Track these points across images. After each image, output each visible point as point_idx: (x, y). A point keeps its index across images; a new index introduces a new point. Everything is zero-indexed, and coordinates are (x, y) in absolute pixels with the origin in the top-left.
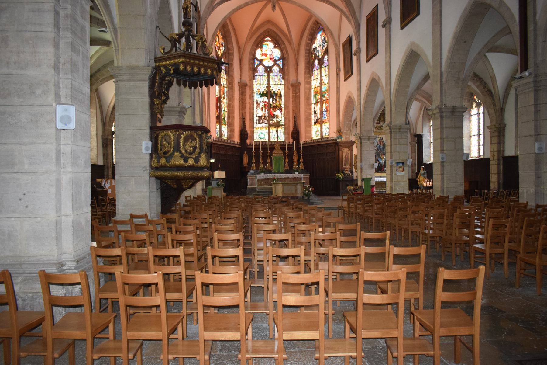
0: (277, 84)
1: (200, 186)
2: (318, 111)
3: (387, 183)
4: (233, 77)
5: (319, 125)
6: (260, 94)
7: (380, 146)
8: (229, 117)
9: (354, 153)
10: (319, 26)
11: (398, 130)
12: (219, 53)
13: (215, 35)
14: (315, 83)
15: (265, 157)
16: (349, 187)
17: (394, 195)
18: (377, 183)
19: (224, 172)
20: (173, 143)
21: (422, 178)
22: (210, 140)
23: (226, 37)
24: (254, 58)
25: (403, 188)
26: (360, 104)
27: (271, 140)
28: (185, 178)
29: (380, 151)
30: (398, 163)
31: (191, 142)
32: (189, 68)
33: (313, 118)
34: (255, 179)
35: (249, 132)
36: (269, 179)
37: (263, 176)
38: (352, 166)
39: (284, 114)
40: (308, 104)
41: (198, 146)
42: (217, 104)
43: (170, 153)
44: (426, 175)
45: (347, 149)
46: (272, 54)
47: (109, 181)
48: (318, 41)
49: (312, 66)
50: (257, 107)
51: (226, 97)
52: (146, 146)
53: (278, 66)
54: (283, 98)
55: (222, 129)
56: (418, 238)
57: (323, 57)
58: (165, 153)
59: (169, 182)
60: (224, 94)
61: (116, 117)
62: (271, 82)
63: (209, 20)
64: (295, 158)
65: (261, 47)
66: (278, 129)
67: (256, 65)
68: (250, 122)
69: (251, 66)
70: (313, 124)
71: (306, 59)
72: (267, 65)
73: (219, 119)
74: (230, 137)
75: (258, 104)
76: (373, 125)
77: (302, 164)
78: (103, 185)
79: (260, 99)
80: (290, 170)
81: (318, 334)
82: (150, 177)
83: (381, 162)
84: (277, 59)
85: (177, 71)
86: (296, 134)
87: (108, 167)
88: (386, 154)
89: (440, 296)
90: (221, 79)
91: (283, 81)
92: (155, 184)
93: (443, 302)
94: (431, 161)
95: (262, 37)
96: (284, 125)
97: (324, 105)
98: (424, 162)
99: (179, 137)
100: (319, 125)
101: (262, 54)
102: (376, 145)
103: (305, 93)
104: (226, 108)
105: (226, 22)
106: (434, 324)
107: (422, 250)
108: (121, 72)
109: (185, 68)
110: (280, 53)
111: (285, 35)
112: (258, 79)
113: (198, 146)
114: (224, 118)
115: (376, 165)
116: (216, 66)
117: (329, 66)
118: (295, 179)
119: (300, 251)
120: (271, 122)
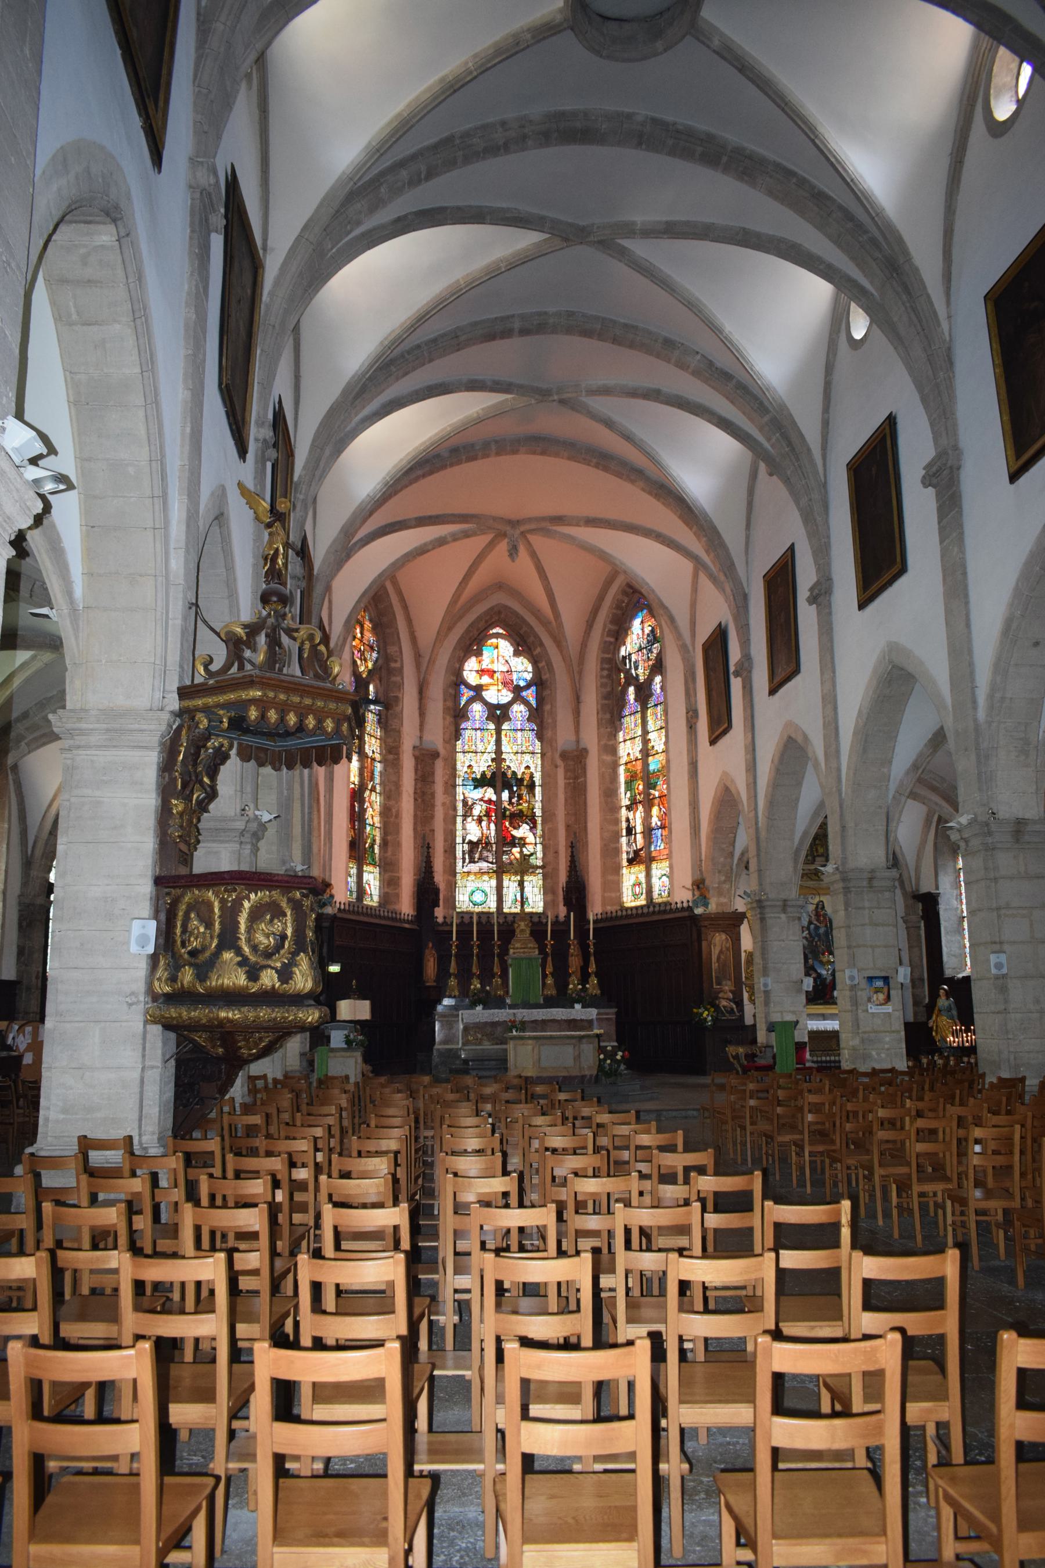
0: (523, 754)
1: (295, 1046)
2: (639, 828)
3: (843, 1036)
4: (399, 732)
5: (642, 867)
6: (474, 780)
7: (817, 928)
8: (384, 844)
9: (743, 948)
10: (633, 599)
11: (865, 883)
12: (362, 669)
13: (353, 622)
14: (628, 750)
15: (486, 957)
16: (731, 1050)
17: (865, 1074)
18: (814, 1035)
19: (366, 1004)
20: (217, 926)
21: (944, 1021)
22: (329, 910)
23: (383, 627)
24: (458, 681)
25: (890, 1053)
26: (756, 809)
27: (506, 910)
28: (248, 1029)
29: (818, 943)
30: (870, 979)
31: (271, 920)
32: (273, 715)
33: (625, 848)
34: (455, 1022)
35: (442, 886)
36: (494, 1024)
37: (480, 1014)
38: (738, 984)
39: (543, 836)
40: (611, 806)
41: (289, 932)
42: (352, 806)
43: (207, 954)
44: (955, 1012)
45: (724, 936)
46: (510, 672)
47: (29, 1029)
48: (635, 637)
49: (620, 702)
50: (465, 816)
52: (143, 932)
53: (526, 703)
54: (538, 790)
55: (366, 877)
56: (940, 1212)
57: (650, 680)
58: (193, 953)
59: (200, 1038)
60: (372, 779)
61: (60, 848)
62: (506, 747)
63: (336, 584)
64: (574, 962)
65: (479, 654)
66: (526, 878)
68: (446, 858)
69: (450, 704)
70: (625, 863)
71: (603, 685)
72: (493, 701)
73: (358, 851)
74: (386, 898)
75: (468, 808)
76: (795, 868)
78: (10, 1041)
79: (476, 794)
80: (562, 999)
81: (635, 1554)
82: (146, 1022)
83: (824, 972)
84: (522, 684)
85: (239, 724)
86: (575, 893)
87: (28, 989)
88: (836, 952)
89: (1012, 1426)
90: (367, 738)
91: (538, 744)
92: (158, 1043)
93: (1020, 1445)
94: (967, 972)
95: (482, 625)
96: (542, 867)
97: (655, 811)
98: (948, 973)
99: (238, 905)
100: (642, 867)
101: (482, 672)
102: (805, 924)
103: (602, 776)
104: (377, 819)
105: (383, 587)
106: (996, 1516)
107: (948, 1266)
108: (84, 726)
109: (263, 716)
110: (530, 668)
111: (545, 623)
113: (289, 932)
114: (372, 846)
115: (809, 983)
116: (350, 711)
117: (665, 703)
118: (572, 1024)
119: (578, 1270)
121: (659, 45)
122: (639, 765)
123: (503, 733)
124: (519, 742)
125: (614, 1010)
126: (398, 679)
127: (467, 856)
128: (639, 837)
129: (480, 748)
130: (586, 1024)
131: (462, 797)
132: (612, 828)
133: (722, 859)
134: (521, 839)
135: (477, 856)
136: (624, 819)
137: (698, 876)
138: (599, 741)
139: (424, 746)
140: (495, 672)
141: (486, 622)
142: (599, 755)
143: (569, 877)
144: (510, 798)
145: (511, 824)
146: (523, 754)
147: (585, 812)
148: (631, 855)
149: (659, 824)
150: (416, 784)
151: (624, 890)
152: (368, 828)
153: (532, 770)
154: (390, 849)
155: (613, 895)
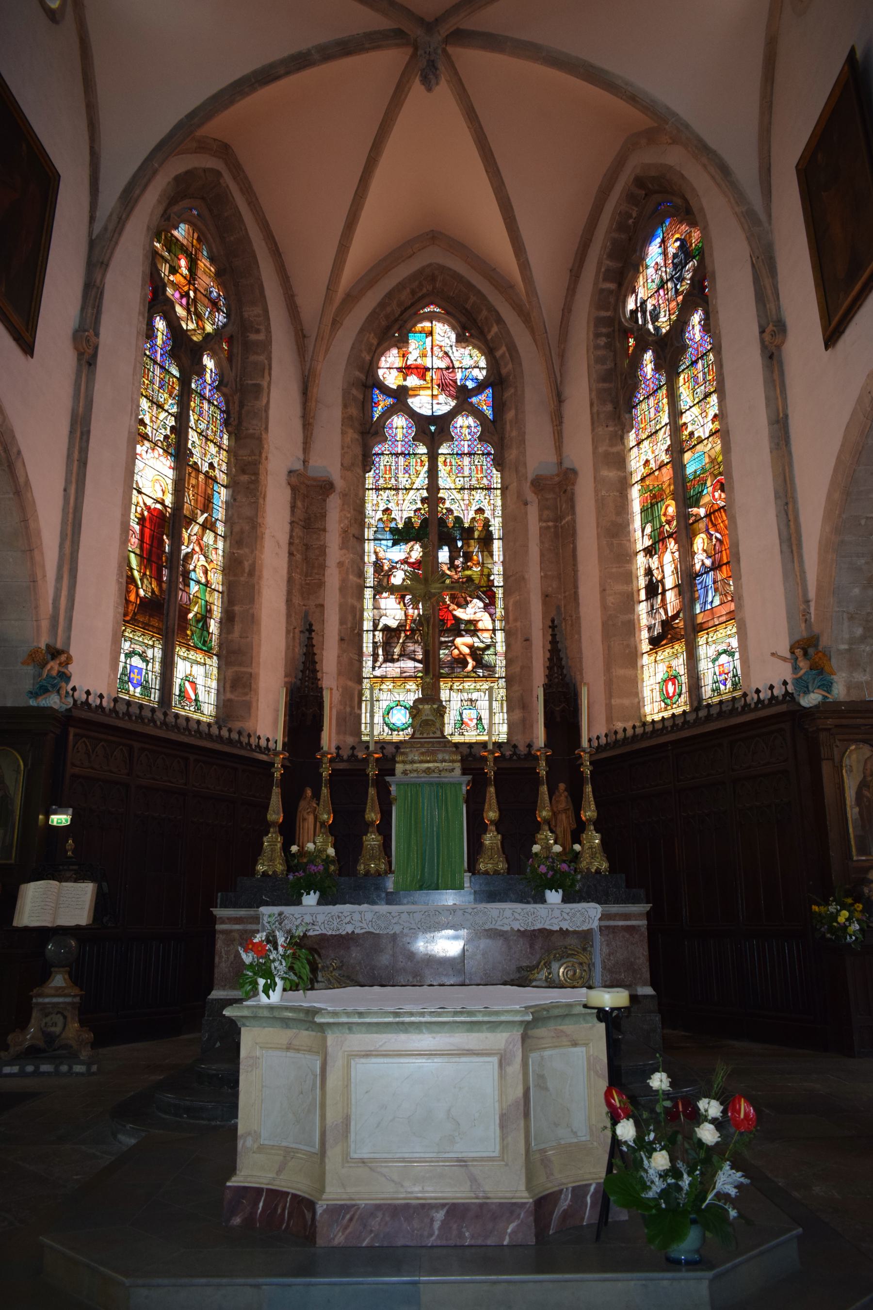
0: (472, 492)
6: (394, 531)
14: (645, 454)
33: (644, 620)
39: (505, 618)
46: (451, 368)
48: (651, 271)
50: (379, 589)
51: (221, 528)
53: (477, 413)
54: (497, 545)
55: (182, 669)
57: (680, 325)
60: (207, 505)
62: (445, 480)
67: (377, 412)
69: (354, 411)
70: (645, 646)
71: (599, 360)
72: (426, 411)
74: (226, 708)
79: (397, 553)
91: (496, 477)
97: (700, 542)
103: (601, 504)
104: (216, 579)
111: (504, 287)
114: (204, 618)
122: (667, 473)
123: (441, 459)
124: (467, 473)
125: (645, 907)
126: (262, 358)
127: (380, 652)
128: (670, 596)
129: (404, 481)
130: (572, 941)
131: (373, 558)
132: (621, 588)
133: (856, 591)
134: (470, 622)
135: (397, 650)
136: (641, 572)
137: (802, 632)
138: (595, 448)
139: (311, 473)
140: (427, 369)
141: (413, 292)
142: (596, 470)
143: (549, 676)
144: (452, 559)
145: (453, 598)
146: (472, 492)
147: (575, 571)
148: (658, 630)
149: (708, 562)
150: (292, 530)
151: (647, 693)
152: (194, 588)
153: (488, 514)
154: (237, 628)
155: (626, 702)
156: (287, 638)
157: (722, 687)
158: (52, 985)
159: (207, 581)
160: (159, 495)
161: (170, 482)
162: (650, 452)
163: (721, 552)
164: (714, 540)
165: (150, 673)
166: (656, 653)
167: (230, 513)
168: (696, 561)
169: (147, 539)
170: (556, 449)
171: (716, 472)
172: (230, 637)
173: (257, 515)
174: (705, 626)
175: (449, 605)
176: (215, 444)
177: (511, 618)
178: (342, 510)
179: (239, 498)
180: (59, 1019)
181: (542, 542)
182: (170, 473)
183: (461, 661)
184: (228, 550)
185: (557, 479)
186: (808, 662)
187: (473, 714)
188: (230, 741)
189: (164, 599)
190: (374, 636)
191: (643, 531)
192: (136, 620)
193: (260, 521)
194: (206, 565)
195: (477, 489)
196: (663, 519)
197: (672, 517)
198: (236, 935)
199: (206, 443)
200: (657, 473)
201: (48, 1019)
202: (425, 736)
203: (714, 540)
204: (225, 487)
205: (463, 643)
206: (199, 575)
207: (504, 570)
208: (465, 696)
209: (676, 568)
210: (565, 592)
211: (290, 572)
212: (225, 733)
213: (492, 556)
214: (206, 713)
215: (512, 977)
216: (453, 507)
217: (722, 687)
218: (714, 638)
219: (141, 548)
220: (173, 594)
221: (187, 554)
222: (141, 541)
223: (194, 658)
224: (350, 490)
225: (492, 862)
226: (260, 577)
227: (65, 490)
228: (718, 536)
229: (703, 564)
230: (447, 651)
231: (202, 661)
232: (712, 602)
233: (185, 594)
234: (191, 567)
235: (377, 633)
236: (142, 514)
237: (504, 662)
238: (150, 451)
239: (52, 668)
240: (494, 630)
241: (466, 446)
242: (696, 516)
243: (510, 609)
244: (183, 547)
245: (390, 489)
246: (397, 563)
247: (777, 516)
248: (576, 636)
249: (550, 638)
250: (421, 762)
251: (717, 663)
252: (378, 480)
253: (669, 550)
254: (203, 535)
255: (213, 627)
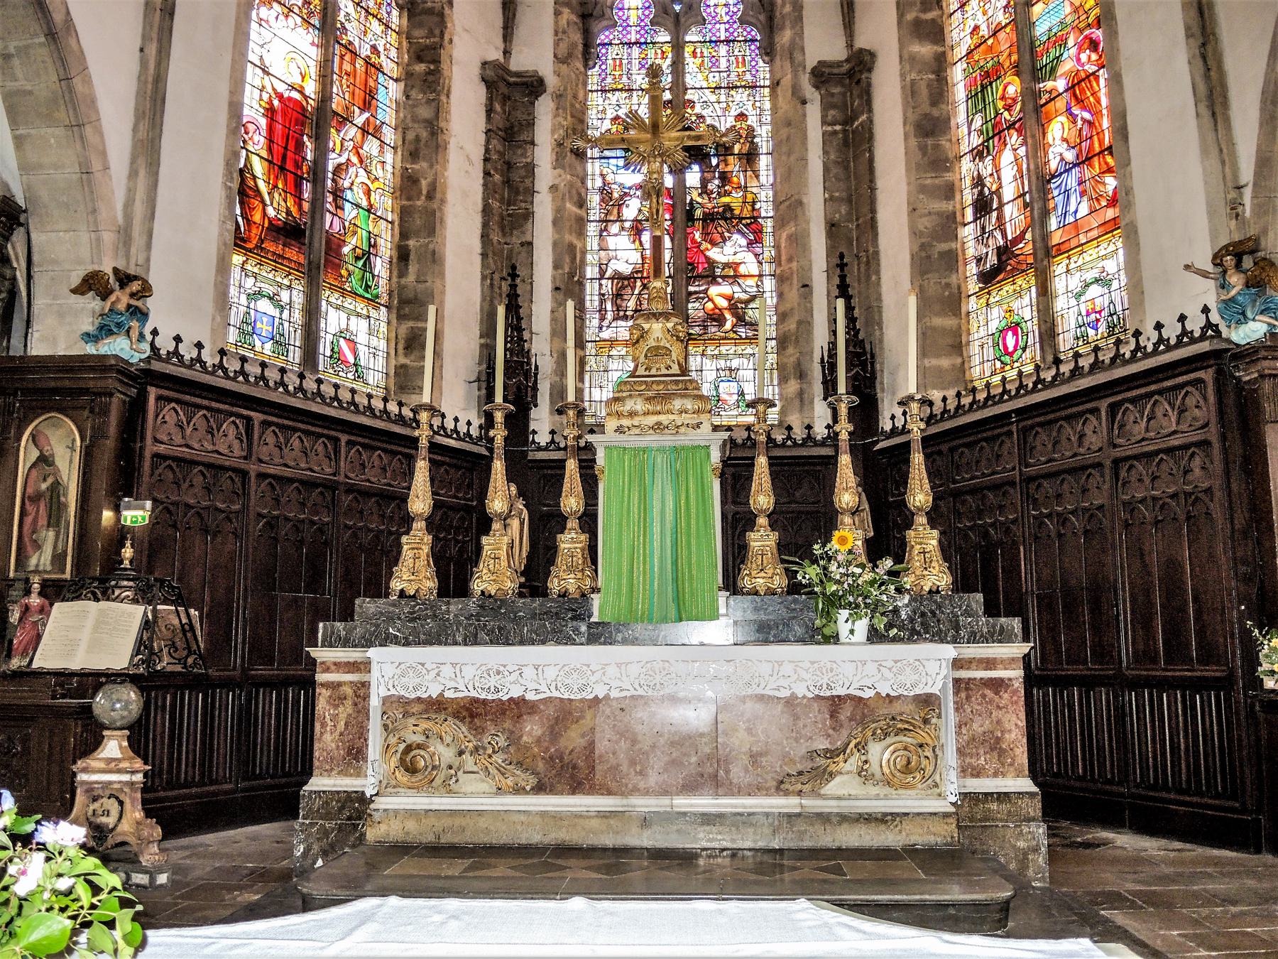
8: (403, 256)
33: (971, 250)
54: (764, 162)
55: (332, 321)
70: (973, 286)
77: (924, 539)
91: (764, 73)
97: (1057, 129)
100: (1027, 283)
103: (911, 92)
104: (385, 203)
112: (618, 64)
114: (366, 256)
120: (693, 308)
121: (910, 129)
123: (688, 49)
124: (723, 64)
127: (609, 306)
128: (1009, 211)
131: (599, 183)
135: (631, 304)
138: (901, 16)
139: (513, 67)
144: (704, 183)
145: (706, 234)
148: (992, 260)
149: (1070, 156)
150: (488, 142)
152: (349, 212)
153: (752, 121)
154: (413, 268)
156: (482, 285)
157: (1091, 332)
158: (102, 755)
159: (371, 206)
160: (297, 80)
161: (312, 64)
162: (979, 14)
163: (1091, 137)
164: (1080, 123)
165: (286, 325)
166: (989, 293)
167: (402, 115)
168: (1051, 156)
169: (279, 139)
170: (845, 28)
171: (1082, 25)
172: (403, 281)
173: (437, 117)
174: (1063, 248)
175: (700, 244)
176: (380, 20)
177: (783, 258)
178: (556, 116)
179: (413, 93)
180: (113, 806)
181: (825, 152)
182: (314, 53)
183: (718, 319)
184: (399, 165)
185: (846, 67)
186: (1242, 275)
187: (733, 387)
188: (400, 419)
189: (305, 224)
190: (601, 285)
191: (970, 124)
192: (262, 249)
193: (442, 124)
194: (369, 183)
195: (736, 87)
196: (1000, 104)
197: (1014, 100)
198: (348, 691)
199: (366, 17)
200: (990, 42)
201: (96, 805)
202: (653, 372)
203: (1080, 123)
204: (396, 80)
205: (719, 293)
206: (358, 195)
207: (775, 196)
208: (722, 363)
209: (1020, 170)
210: (857, 220)
211: (485, 199)
212: (393, 407)
213: (757, 177)
214: (371, 382)
215: (800, 767)
216: (704, 113)
217: (1091, 332)
218: (1080, 263)
219: (270, 150)
220: (318, 216)
221: (339, 165)
222: (270, 139)
223: (352, 307)
224: (565, 89)
225: (765, 572)
226: (443, 201)
227: (142, 50)
228: (1087, 116)
229: (1062, 159)
230: (697, 305)
231: (365, 312)
232: (1076, 212)
233: (336, 219)
234: (347, 184)
235: (604, 282)
236: (270, 102)
237: (775, 318)
238: (281, 17)
239: (118, 300)
240: (760, 276)
241: (723, 30)
242: (1050, 92)
243: (783, 245)
244: (332, 155)
245: (621, 90)
246: (630, 188)
247: (1190, 63)
248: (874, 278)
249: (837, 281)
250: (647, 413)
251: (1083, 299)
252: (604, 79)
253: (1009, 146)
254: (363, 142)
255: (380, 267)
